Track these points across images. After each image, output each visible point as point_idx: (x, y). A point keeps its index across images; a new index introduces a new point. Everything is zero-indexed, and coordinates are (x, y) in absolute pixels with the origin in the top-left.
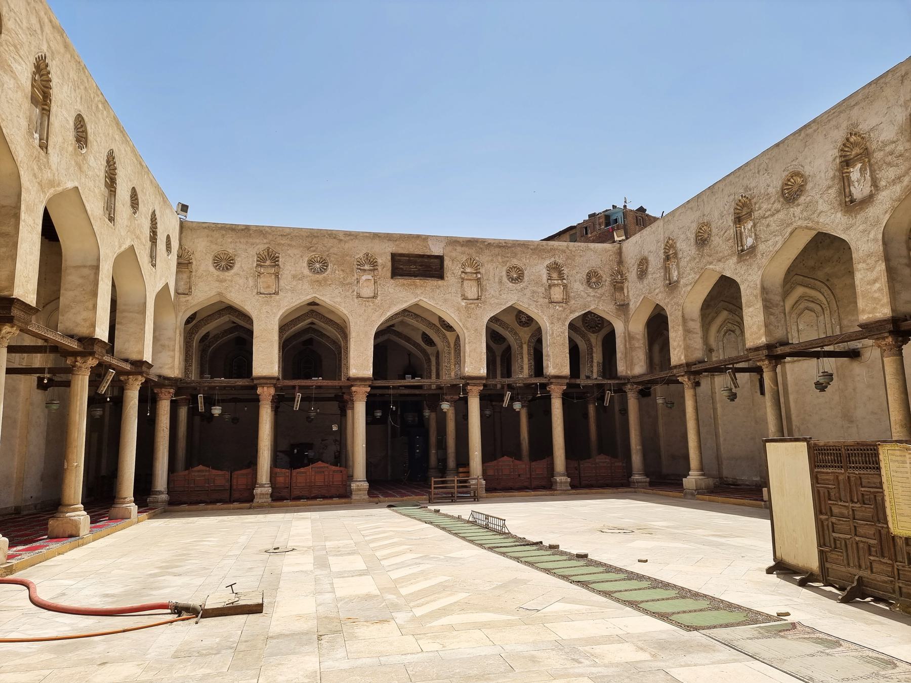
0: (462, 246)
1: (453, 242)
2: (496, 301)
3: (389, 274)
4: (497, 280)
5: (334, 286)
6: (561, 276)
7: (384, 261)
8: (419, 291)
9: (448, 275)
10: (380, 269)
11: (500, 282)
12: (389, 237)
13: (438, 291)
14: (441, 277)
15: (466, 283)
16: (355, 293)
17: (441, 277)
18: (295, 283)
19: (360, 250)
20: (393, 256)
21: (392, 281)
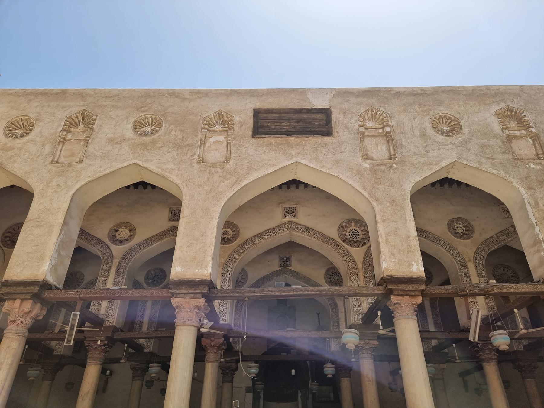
0: (357, 96)
1: (344, 94)
2: (422, 160)
3: (250, 132)
4: (417, 132)
5: (165, 149)
6: (523, 124)
7: (244, 119)
8: (294, 152)
9: (338, 129)
10: (236, 127)
11: (423, 135)
12: (252, 93)
13: (324, 150)
14: (329, 133)
15: (367, 141)
16: (196, 157)
17: (329, 133)
18: (109, 148)
19: (211, 109)
20: (255, 110)
21: (253, 140)
